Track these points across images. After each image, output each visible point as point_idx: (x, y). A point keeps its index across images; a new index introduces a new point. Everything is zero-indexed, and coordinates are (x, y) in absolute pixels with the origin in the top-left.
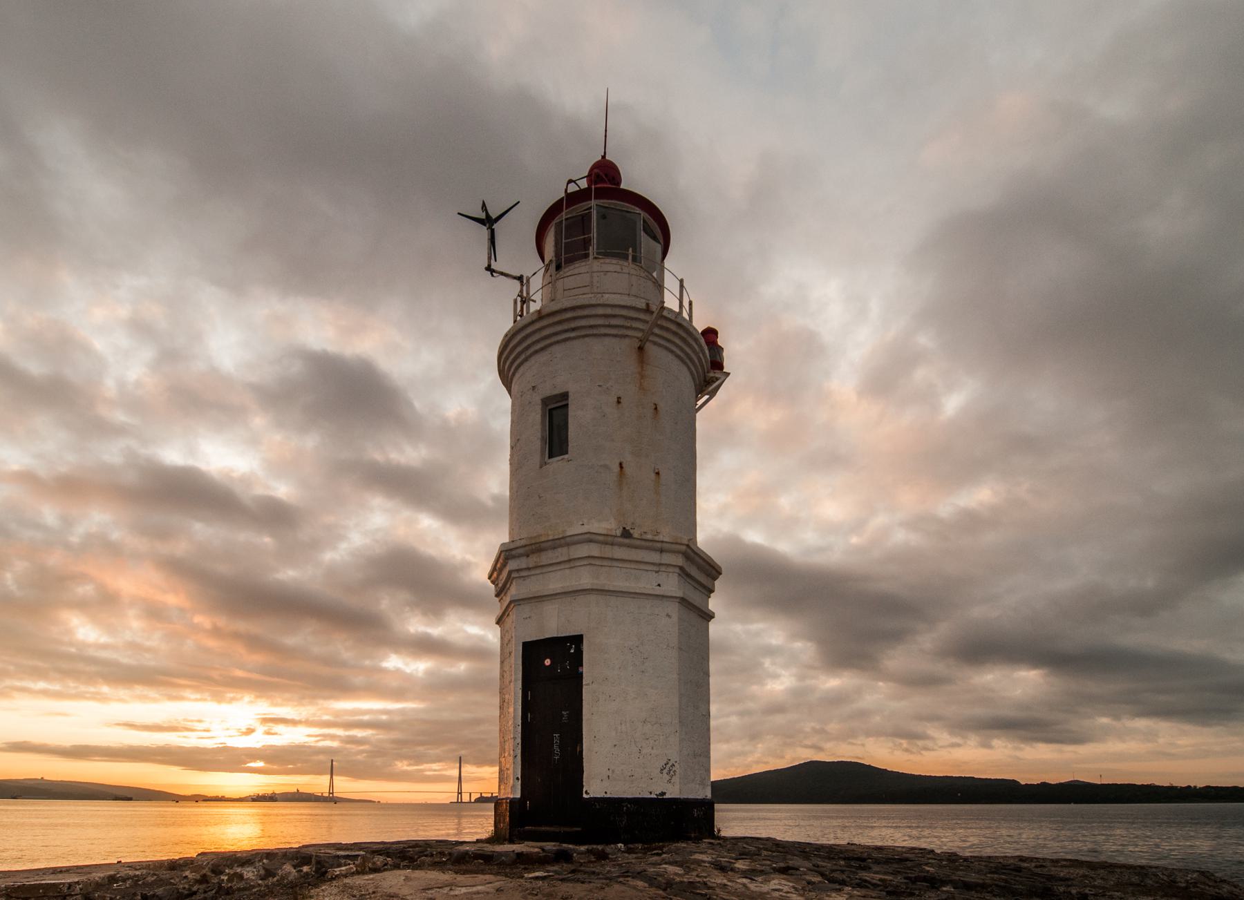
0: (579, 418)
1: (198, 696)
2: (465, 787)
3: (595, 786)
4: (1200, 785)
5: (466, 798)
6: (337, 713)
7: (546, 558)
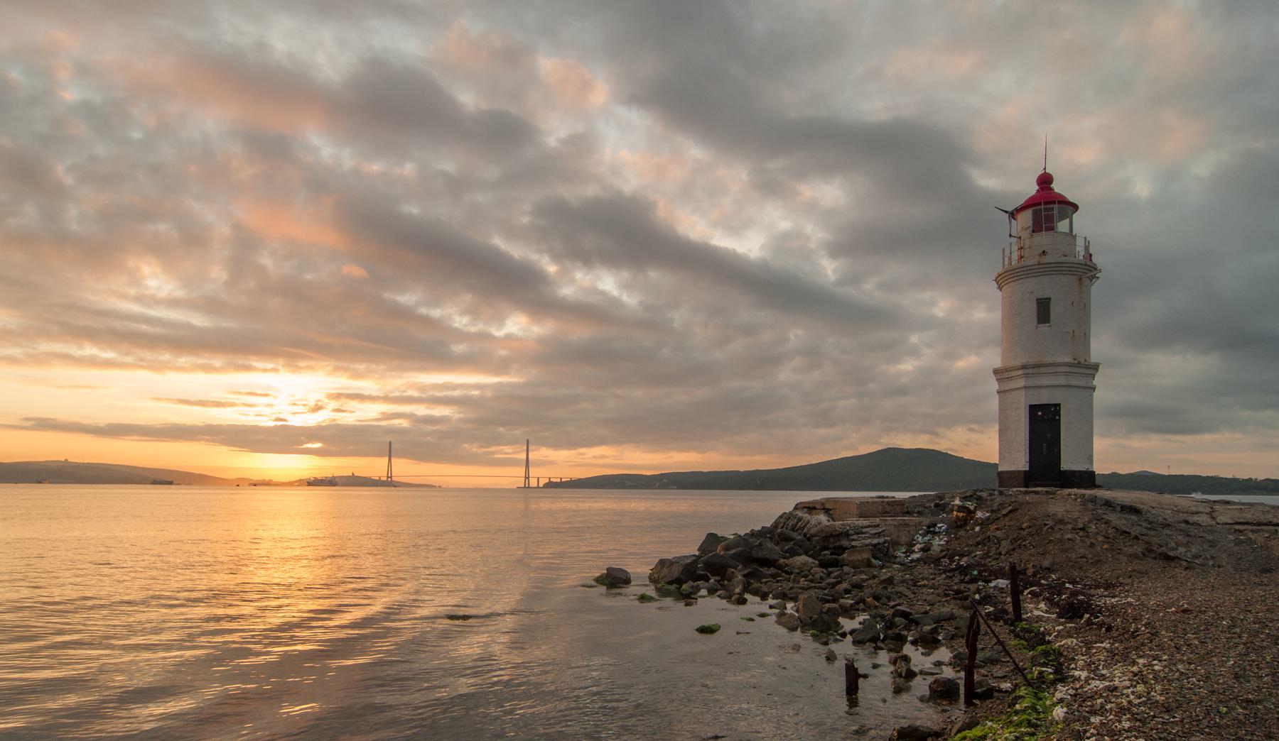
0: (1055, 310)
1: (270, 366)
2: (534, 472)
3: (1065, 466)
4: (1261, 477)
5: (533, 483)
6: (423, 388)
7: (1043, 370)
